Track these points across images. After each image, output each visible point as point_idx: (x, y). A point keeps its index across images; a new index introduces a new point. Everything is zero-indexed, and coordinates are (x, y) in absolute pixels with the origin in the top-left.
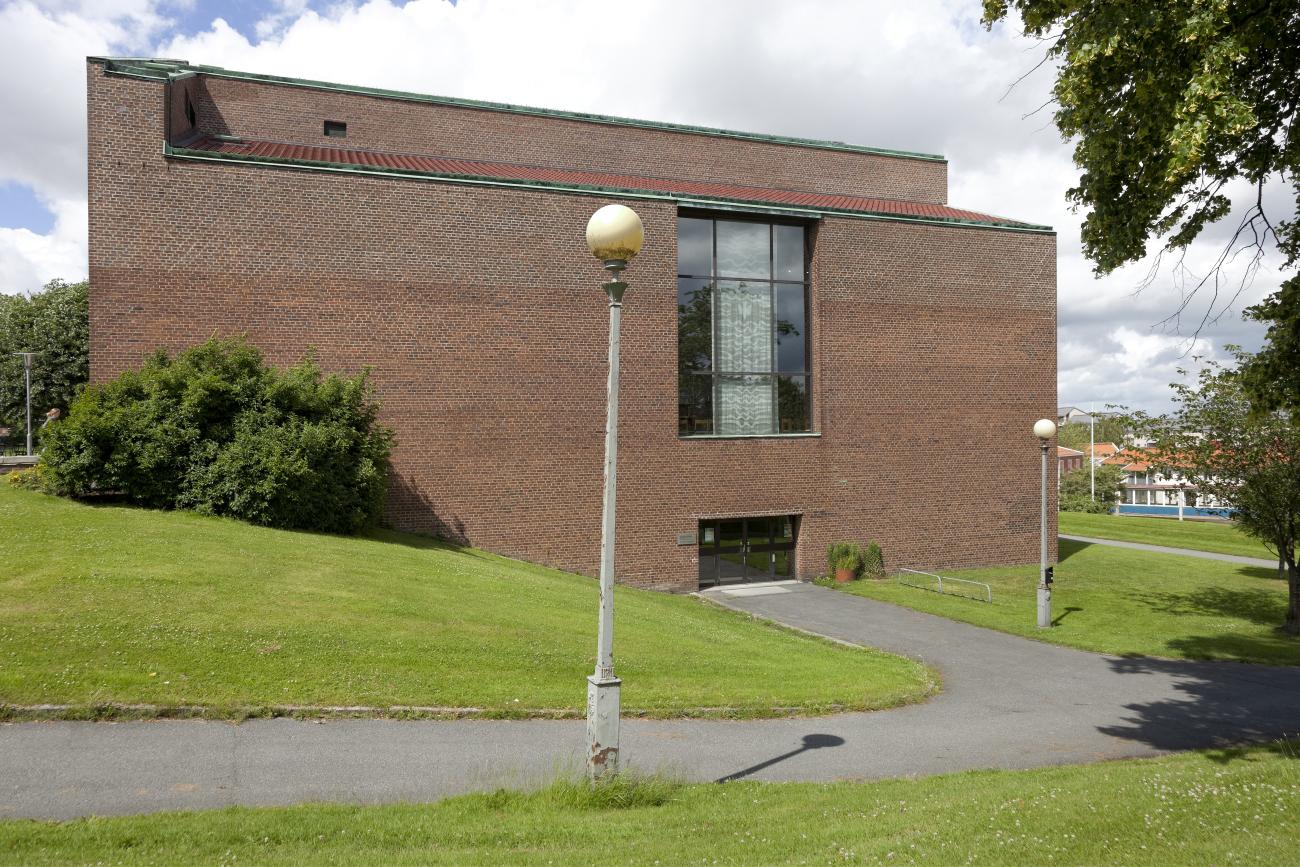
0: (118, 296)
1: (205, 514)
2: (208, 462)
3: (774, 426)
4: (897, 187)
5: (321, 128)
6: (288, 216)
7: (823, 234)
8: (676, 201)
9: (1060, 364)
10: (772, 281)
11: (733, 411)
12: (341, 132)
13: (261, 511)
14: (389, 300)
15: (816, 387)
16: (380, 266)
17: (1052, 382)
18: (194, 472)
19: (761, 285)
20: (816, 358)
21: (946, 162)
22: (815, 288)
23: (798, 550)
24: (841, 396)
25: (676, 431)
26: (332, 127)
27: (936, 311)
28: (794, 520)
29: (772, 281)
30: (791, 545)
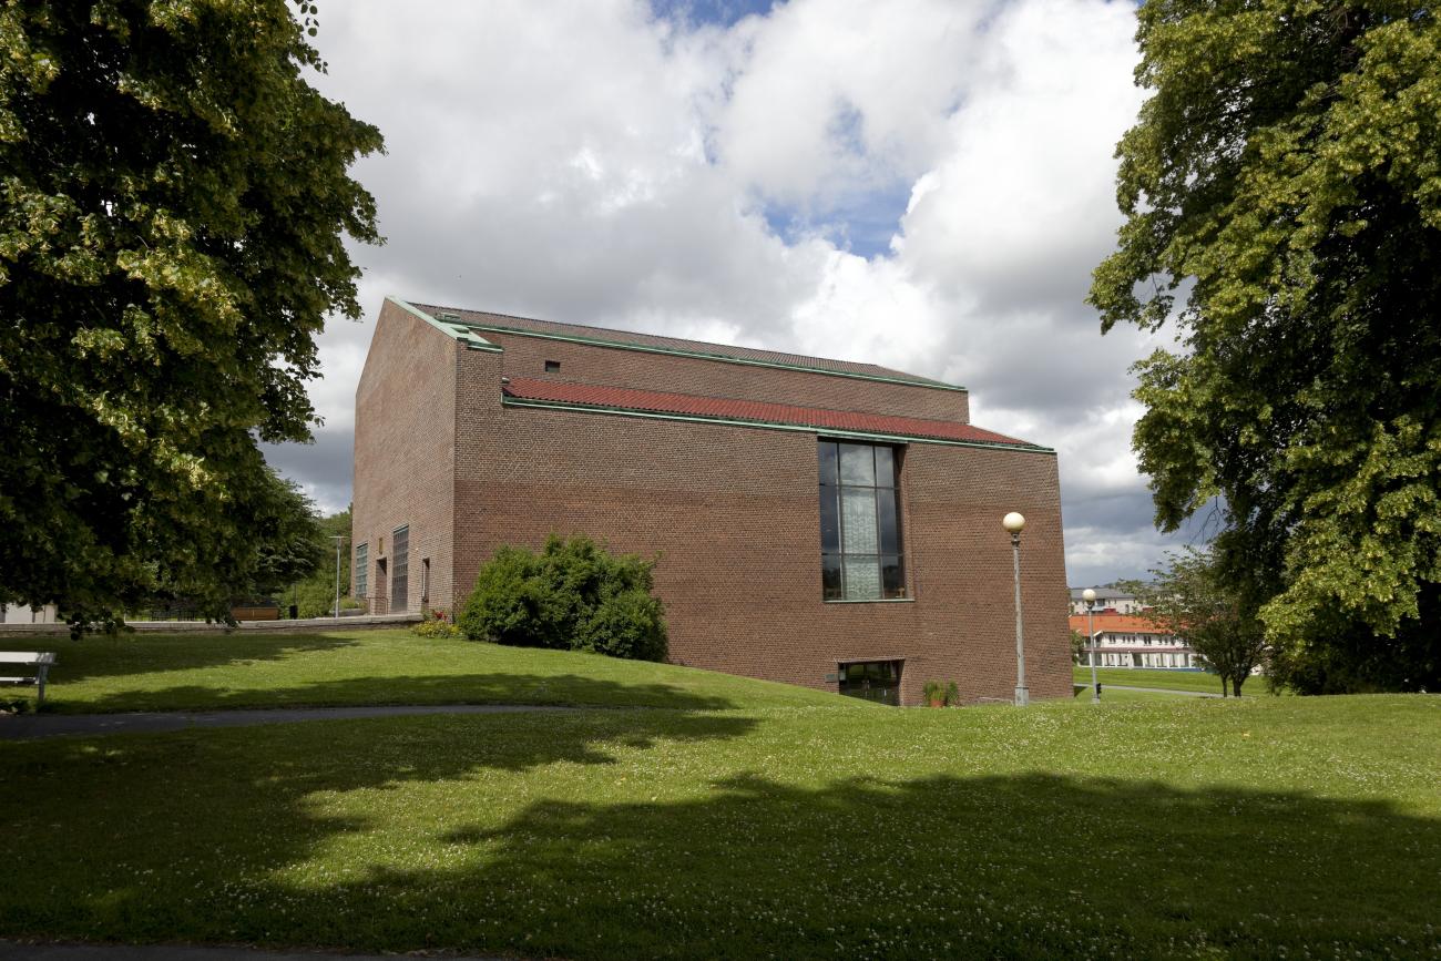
0: (471, 500)
1: (589, 652)
2: (589, 617)
3: (881, 592)
4: (935, 409)
5: (543, 365)
6: (576, 444)
7: (910, 455)
8: (816, 432)
9: (1065, 542)
10: (876, 488)
11: (854, 583)
12: (555, 369)
13: (626, 650)
14: (639, 502)
15: (908, 565)
16: (633, 478)
17: (1060, 560)
18: (581, 624)
19: (869, 490)
20: (907, 544)
21: (966, 392)
22: (904, 493)
23: (902, 687)
24: (927, 571)
25: (821, 596)
26: (550, 365)
27: (984, 509)
28: (898, 665)
29: (876, 488)
30: (897, 683)
